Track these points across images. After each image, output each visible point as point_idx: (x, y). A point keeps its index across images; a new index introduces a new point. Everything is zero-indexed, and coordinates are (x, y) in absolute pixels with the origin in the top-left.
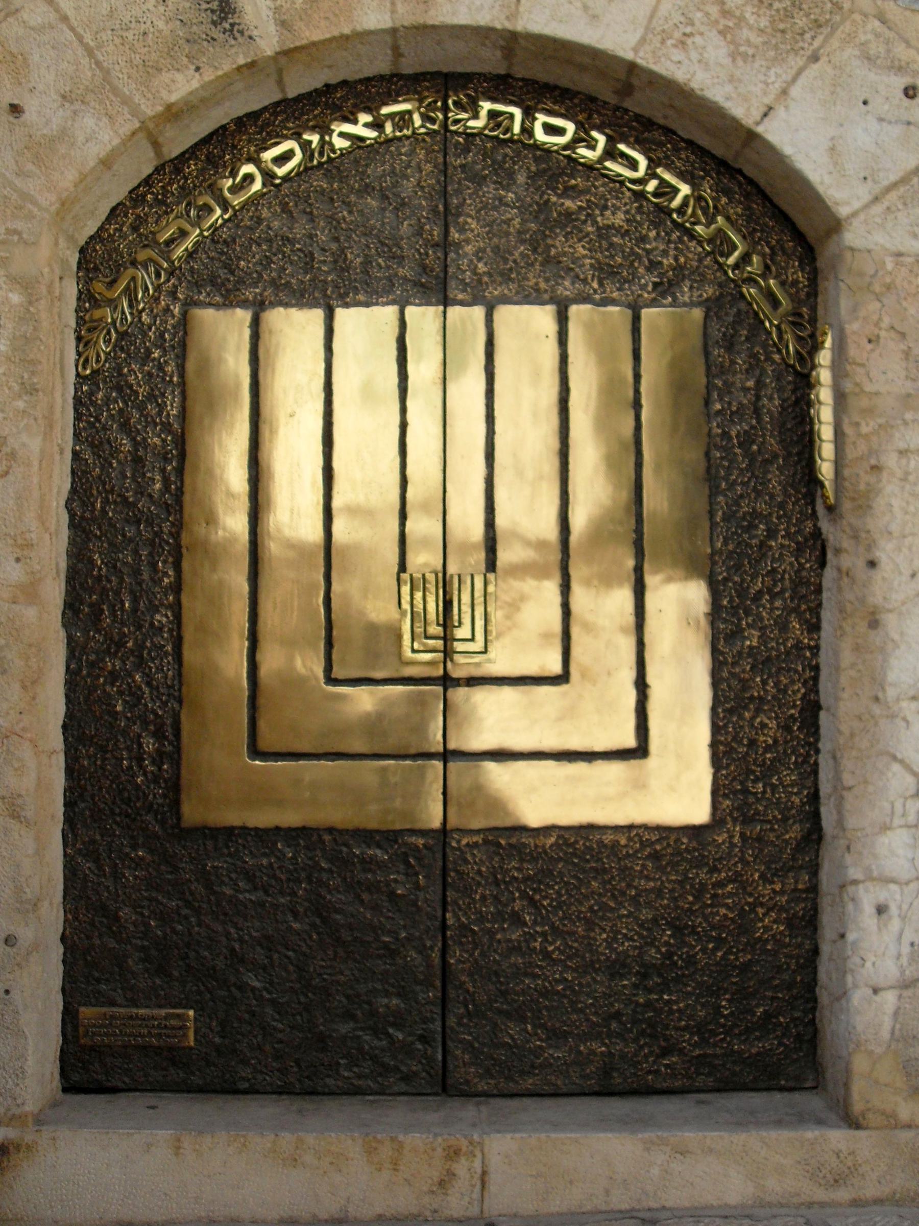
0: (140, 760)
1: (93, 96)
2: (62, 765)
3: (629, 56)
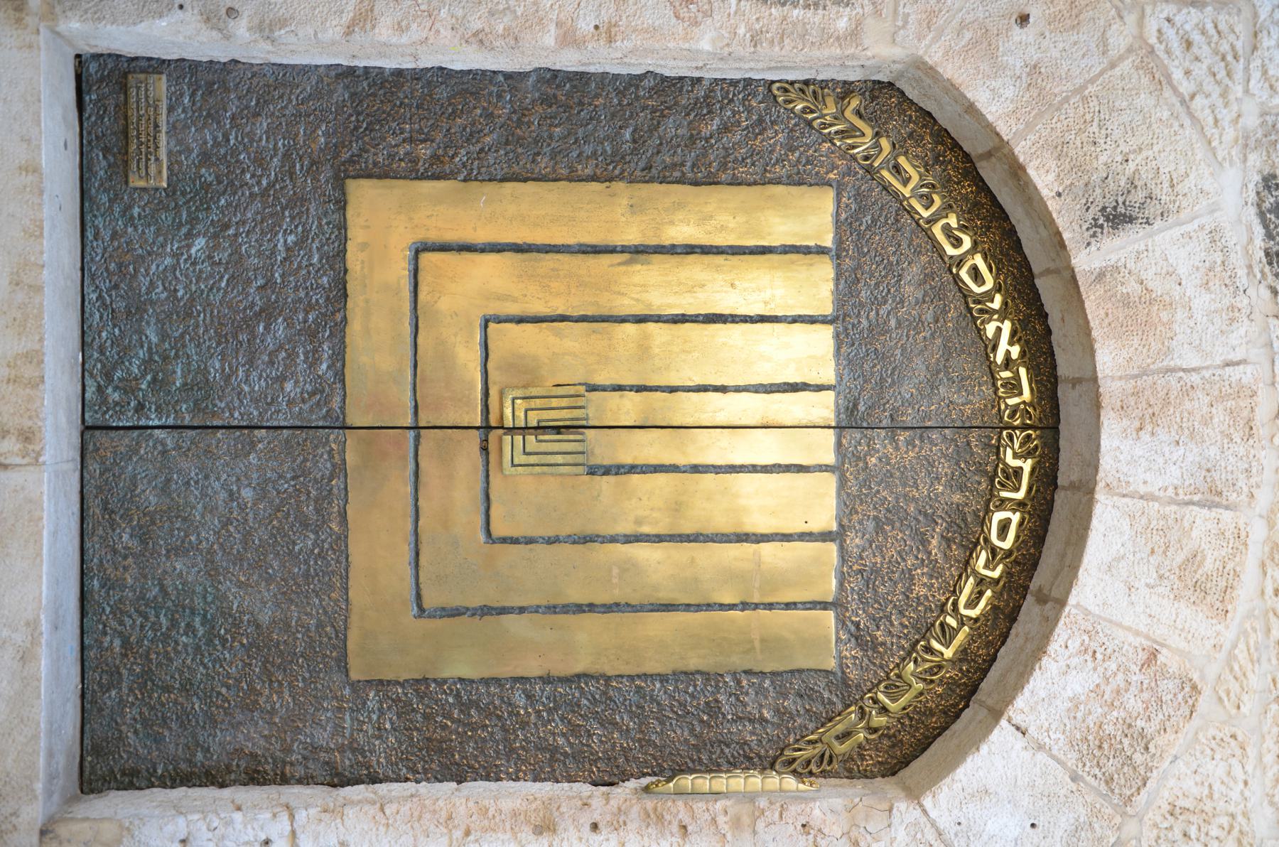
0: (411, 140)
1: (1035, 95)
2: (404, 66)
3: (1072, 600)
